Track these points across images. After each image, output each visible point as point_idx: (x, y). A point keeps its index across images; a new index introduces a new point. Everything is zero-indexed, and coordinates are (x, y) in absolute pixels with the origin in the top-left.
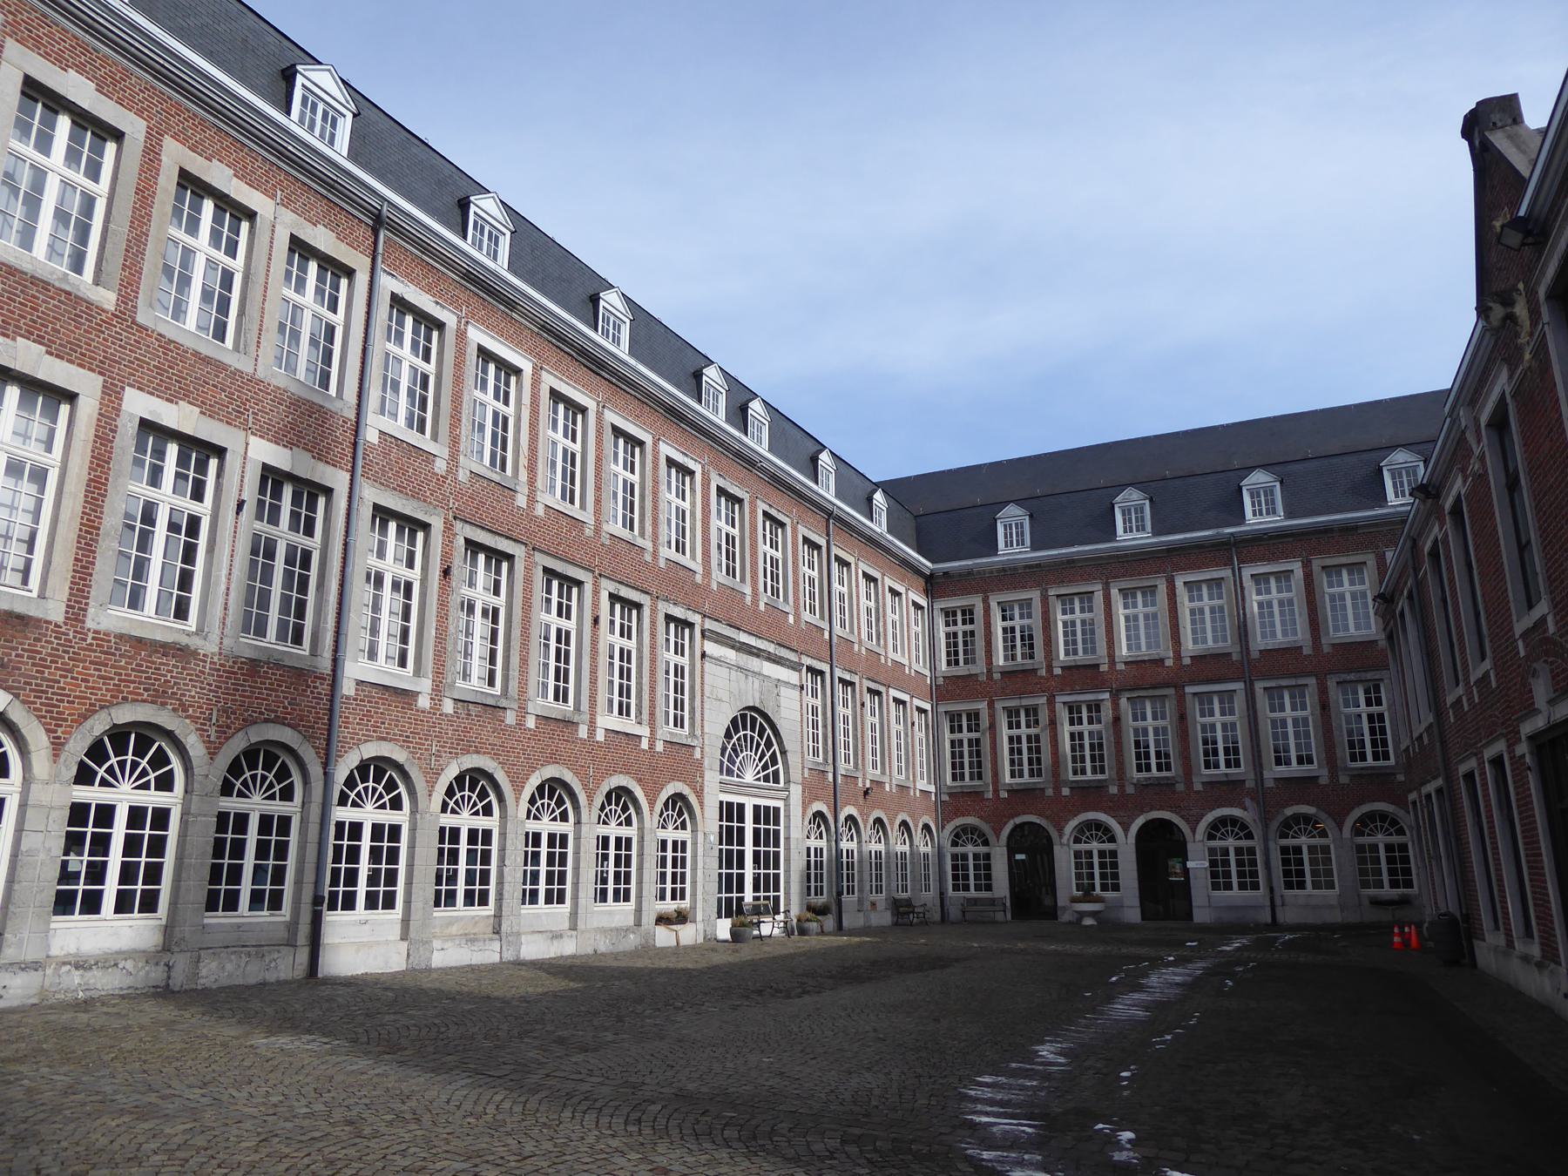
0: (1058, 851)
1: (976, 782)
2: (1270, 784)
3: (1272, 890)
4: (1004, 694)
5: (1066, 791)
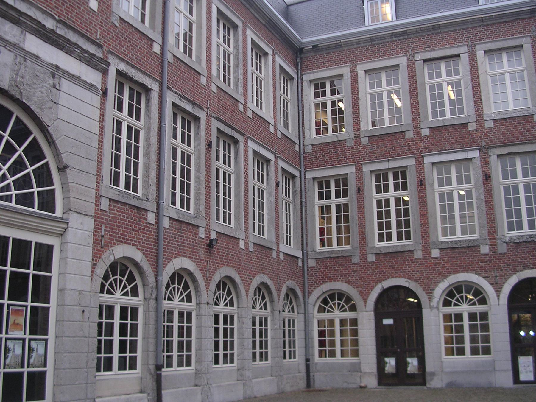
1: (344, 247)
4: (373, 158)
5: (435, 253)
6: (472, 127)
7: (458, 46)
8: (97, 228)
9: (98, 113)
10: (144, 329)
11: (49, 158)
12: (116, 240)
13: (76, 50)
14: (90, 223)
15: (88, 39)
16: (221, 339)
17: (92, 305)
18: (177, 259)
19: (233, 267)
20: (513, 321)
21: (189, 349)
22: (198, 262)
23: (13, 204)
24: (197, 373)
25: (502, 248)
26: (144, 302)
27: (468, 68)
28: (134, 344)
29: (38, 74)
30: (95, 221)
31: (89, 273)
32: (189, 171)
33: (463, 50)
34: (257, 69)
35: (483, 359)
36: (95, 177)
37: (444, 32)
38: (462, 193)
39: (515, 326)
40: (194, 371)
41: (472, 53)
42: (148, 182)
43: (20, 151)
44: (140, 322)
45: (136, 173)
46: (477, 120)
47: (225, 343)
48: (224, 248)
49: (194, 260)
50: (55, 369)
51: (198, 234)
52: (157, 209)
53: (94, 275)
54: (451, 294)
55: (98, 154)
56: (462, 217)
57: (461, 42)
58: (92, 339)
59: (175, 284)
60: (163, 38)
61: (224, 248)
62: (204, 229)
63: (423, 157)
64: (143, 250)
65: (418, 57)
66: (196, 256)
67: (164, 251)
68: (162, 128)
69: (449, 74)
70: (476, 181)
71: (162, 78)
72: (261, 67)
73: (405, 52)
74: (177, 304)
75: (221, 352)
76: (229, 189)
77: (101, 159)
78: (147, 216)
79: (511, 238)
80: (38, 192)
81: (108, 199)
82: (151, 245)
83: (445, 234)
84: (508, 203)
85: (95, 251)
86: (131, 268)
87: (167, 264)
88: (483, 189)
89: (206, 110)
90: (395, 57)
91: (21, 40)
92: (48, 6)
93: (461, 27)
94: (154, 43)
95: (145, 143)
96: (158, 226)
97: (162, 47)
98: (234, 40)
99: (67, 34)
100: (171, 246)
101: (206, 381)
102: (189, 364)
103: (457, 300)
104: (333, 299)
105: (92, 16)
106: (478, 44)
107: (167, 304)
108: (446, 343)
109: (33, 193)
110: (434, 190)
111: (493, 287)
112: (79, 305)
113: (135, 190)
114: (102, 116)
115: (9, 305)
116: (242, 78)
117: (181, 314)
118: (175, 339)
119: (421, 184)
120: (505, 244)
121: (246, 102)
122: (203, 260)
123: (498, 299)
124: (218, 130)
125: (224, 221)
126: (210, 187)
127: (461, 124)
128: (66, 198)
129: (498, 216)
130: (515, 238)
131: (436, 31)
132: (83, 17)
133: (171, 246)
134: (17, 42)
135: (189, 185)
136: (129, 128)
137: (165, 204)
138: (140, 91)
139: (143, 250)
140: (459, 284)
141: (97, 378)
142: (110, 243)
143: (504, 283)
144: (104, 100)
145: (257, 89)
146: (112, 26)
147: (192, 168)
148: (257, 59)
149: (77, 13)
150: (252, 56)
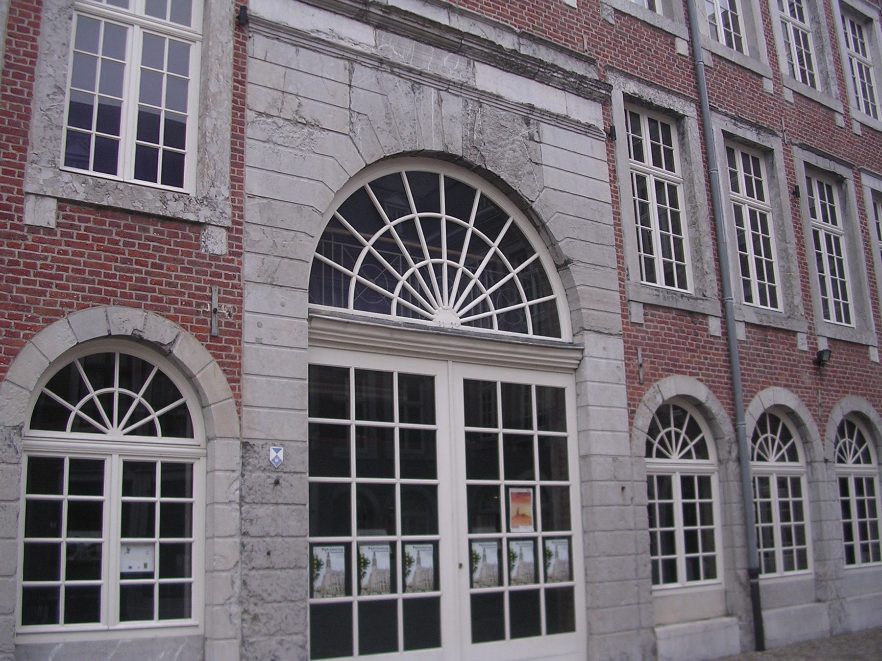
8: (630, 353)
9: (605, 168)
10: (724, 511)
11: (541, 252)
12: (663, 370)
13: (555, 74)
14: (617, 347)
15: (572, 54)
16: (855, 520)
17: (636, 477)
18: (765, 390)
19: (862, 395)
21: (801, 540)
22: (802, 392)
23: (496, 330)
24: (819, 580)
26: (807, 468)
28: (708, 536)
29: (503, 123)
30: (625, 342)
31: (625, 426)
32: (767, 241)
34: (857, 50)
35: (800, 578)
36: (616, 272)
40: (813, 577)
42: (703, 268)
43: (495, 246)
44: (716, 499)
45: (680, 256)
47: (863, 526)
48: (844, 363)
49: (795, 390)
50: (587, 582)
51: (796, 345)
52: (722, 311)
53: (634, 429)
55: (616, 235)
58: (640, 532)
59: (670, 426)
60: (690, 29)
61: (844, 363)
62: (805, 336)
64: (708, 381)
66: (798, 382)
67: (743, 380)
68: (712, 176)
71: (699, 93)
72: (863, 44)
74: (773, 466)
75: (857, 542)
76: (840, 262)
77: (621, 241)
78: (707, 325)
80: (531, 307)
81: (641, 305)
82: (720, 371)
85: (631, 390)
86: (692, 412)
87: (749, 401)
89: (781, 134)
91: (469, 75)
92: (499, 14)
94: (677, 39)
95: (689, 205)
96: (727, 340)
97: (691, 43)
98: (809, 8)
99: (537, 52)
100: (753, 371)
101: (834, 594)
102: (803, 565)
104: (102, 378)
105: (569, 16)
107: (757, 467)
109: (523, 309)
112: (615, 479)
113: (683, 284)
114: (613, 171)
115: (507, 487)
116: (834, 70)
117: (782, 483)
118: (777, 524)
121: (847, 111)
122: (810, 388)
124: (807, 165)
125: (839, 319)
126: (806, 264)
128: (575, 311)
132: (557, 21)
133: (753, 371)
134: (464, 80)
135: (770, 265)
136: (659, 185)
137: (734, 301)
138: (667, 122)
139: (708, 381)
141: (655, 594)
142: (653, 375)
144: (612, 146)
145: (863, 85)
146: (605, 26)
147: (772, 235)
148: (854, 32)
149: (546, 16)
150: (845, 28)
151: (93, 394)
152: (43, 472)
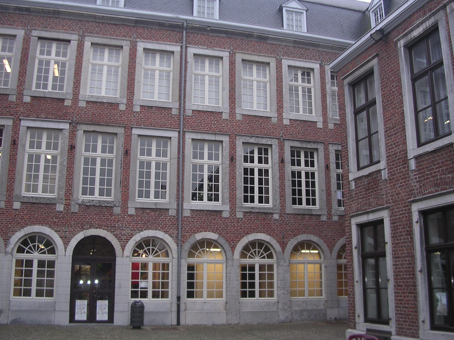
0: (119, 261)
2: (187, 214)
3: (179, 298)
5: (17, 205)
6: (68, 103)
7: (71, 33)
20: (75, 270)
25: (75, 209)
27: (75, 54)
33: (74, 37)
35: (46, 300)
37: (62, 19)
38: (49, 157)
39: (76, 275)
41: (81, 42)
46: (73, 98)
54: (25, 243)
56: (45, 178)
57: (74, 31)
63: (20, 120)
65: (35, 33)
69: (58, 54)
70: (62, 148)
73: (24, 26)
79: (83, 201)
83: (28, 190)
84: (86, 171)
88: (67, 157)
90: (15, 28)
93: (77, 18)
103: (30, 248)
104: (260, 247)
106: (87, 36)
108: (15, 285)
110: (25, 150)
111: (62, 240)
119: (14, 143)
120: (78, 205)
123: (65, 250)
127: (59, 99)
129: (75, 181)
130: (86, 201)
131: (56, 16)
140: (203, 240)
143: (72, 238)
151: (31, 245)
152: (243, 268)
